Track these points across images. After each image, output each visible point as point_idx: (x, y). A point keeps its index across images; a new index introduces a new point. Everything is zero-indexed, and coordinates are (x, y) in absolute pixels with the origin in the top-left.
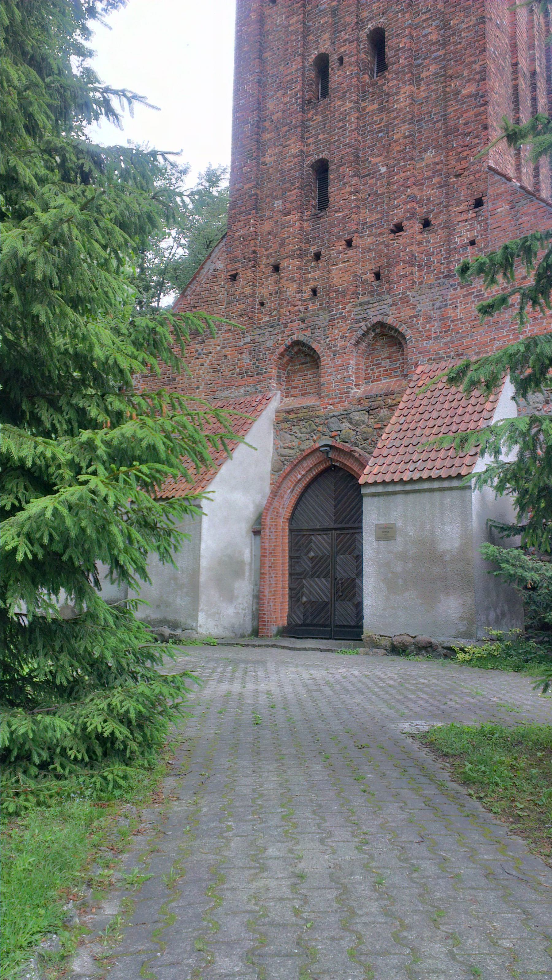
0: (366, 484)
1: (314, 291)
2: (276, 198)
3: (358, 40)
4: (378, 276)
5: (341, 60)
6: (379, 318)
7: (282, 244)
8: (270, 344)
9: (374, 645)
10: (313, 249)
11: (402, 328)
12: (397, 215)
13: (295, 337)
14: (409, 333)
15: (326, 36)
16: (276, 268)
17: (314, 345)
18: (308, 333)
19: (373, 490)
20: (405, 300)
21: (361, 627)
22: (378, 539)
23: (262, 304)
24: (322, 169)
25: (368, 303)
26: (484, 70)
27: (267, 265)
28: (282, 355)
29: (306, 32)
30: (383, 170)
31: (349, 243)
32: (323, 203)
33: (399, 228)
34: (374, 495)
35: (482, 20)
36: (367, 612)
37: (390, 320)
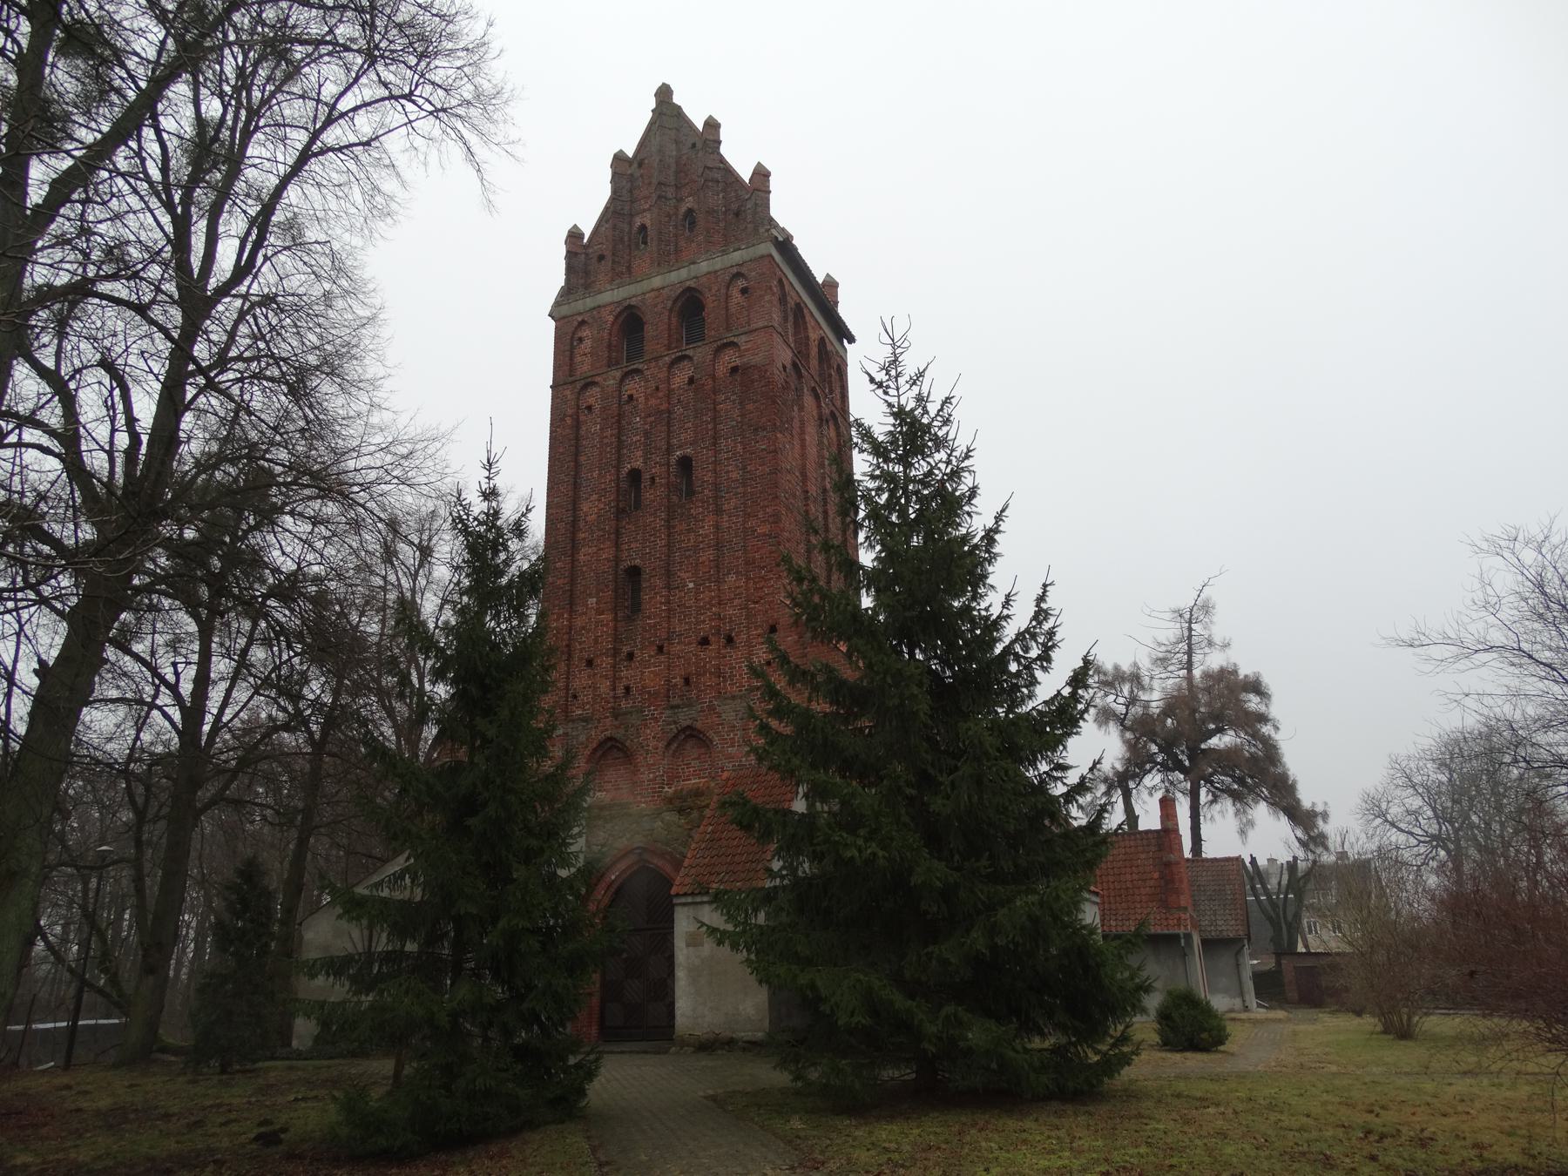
0: (678, 895)
1: (627, 689)
2: (590, 596)
3: (668, 465)
4: (687, 681)
5: (653, 479)
6: (689, 722)
7: (596, 641)
8: (582, 738)
9: (683, 1043)
10: (626, 649)
11: (711, 734)
12: (705, 628)
13: (608, 733)
14: (716, 740)
15: (640, 453)
16: (590, 663)
17: (628, 743)
18: (622, 731)
19: (683, 900)
20: (711, 708)
21: (673, 1026)
22: (688, 945)
23: (575, 697)
24: (634, 572)
25: (678, 707)
26: (776, 812)
27: (581, 659)
28: (595, 750)
29: (620, 445)
30: (691, 585)
31: (660, 649)
32: (636, 607)
33: (705, 642)
34: (684, 904)
35: (776, 471)
36: (678, 1013)
37: (698, 725)
